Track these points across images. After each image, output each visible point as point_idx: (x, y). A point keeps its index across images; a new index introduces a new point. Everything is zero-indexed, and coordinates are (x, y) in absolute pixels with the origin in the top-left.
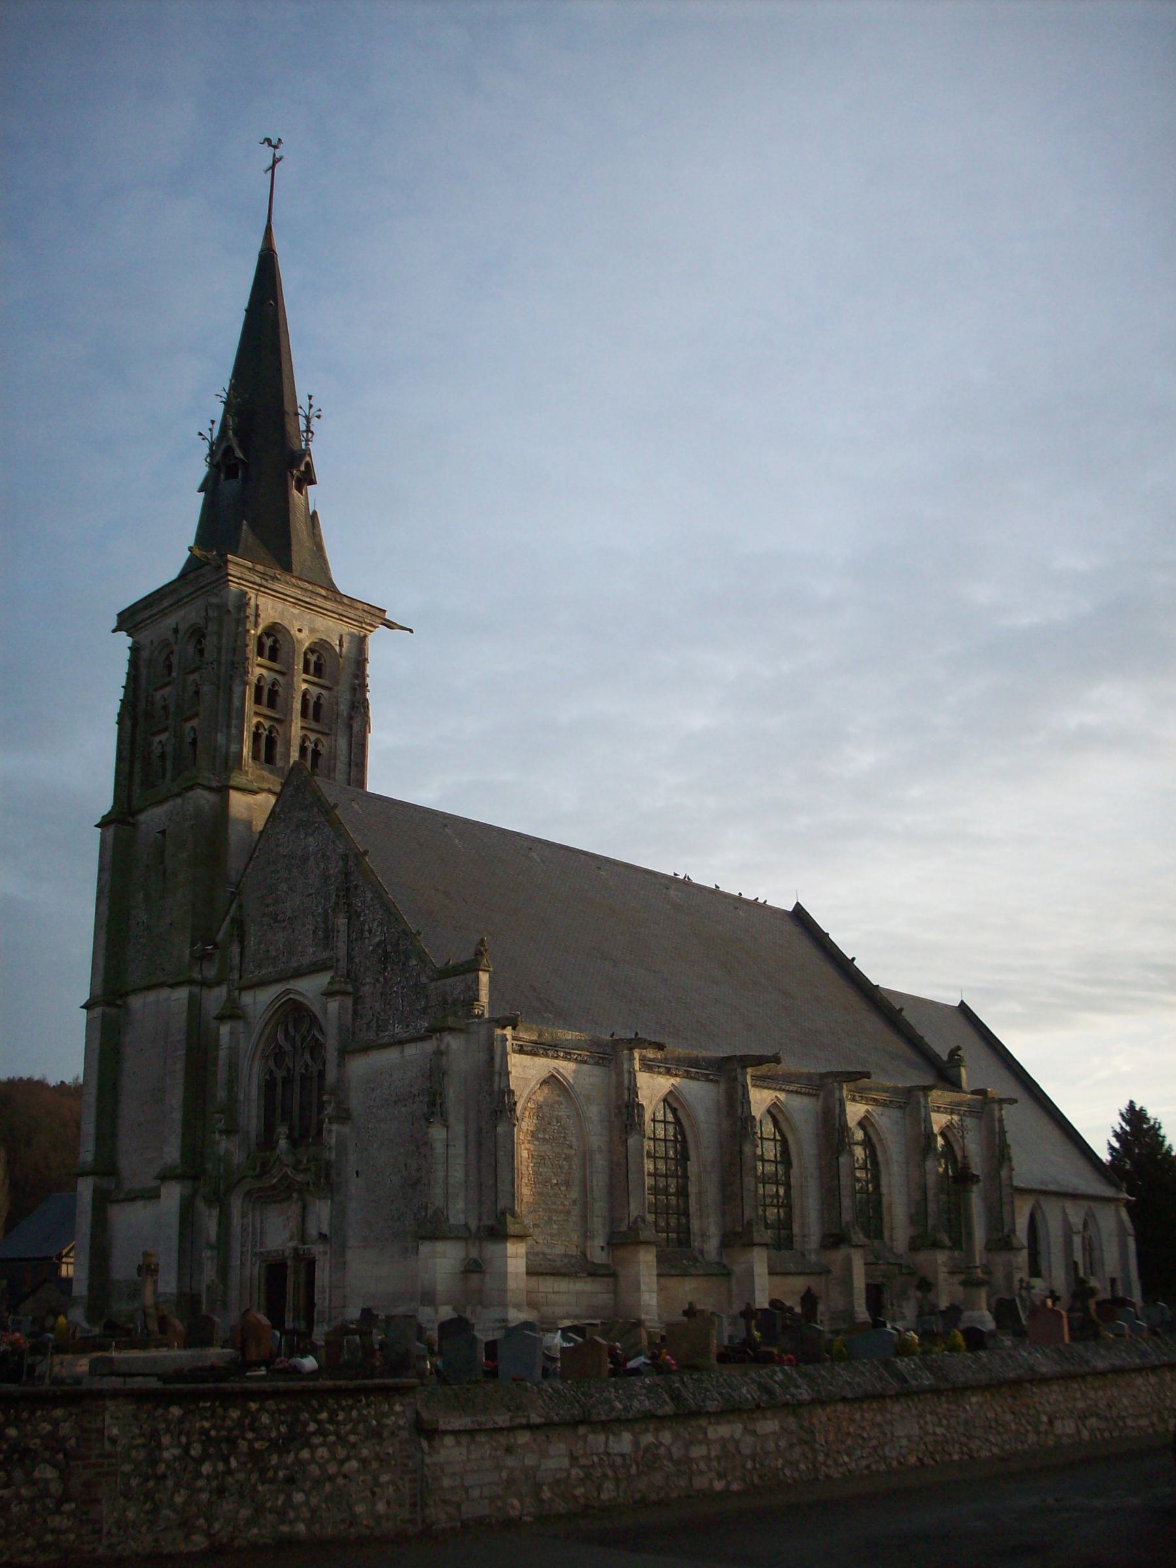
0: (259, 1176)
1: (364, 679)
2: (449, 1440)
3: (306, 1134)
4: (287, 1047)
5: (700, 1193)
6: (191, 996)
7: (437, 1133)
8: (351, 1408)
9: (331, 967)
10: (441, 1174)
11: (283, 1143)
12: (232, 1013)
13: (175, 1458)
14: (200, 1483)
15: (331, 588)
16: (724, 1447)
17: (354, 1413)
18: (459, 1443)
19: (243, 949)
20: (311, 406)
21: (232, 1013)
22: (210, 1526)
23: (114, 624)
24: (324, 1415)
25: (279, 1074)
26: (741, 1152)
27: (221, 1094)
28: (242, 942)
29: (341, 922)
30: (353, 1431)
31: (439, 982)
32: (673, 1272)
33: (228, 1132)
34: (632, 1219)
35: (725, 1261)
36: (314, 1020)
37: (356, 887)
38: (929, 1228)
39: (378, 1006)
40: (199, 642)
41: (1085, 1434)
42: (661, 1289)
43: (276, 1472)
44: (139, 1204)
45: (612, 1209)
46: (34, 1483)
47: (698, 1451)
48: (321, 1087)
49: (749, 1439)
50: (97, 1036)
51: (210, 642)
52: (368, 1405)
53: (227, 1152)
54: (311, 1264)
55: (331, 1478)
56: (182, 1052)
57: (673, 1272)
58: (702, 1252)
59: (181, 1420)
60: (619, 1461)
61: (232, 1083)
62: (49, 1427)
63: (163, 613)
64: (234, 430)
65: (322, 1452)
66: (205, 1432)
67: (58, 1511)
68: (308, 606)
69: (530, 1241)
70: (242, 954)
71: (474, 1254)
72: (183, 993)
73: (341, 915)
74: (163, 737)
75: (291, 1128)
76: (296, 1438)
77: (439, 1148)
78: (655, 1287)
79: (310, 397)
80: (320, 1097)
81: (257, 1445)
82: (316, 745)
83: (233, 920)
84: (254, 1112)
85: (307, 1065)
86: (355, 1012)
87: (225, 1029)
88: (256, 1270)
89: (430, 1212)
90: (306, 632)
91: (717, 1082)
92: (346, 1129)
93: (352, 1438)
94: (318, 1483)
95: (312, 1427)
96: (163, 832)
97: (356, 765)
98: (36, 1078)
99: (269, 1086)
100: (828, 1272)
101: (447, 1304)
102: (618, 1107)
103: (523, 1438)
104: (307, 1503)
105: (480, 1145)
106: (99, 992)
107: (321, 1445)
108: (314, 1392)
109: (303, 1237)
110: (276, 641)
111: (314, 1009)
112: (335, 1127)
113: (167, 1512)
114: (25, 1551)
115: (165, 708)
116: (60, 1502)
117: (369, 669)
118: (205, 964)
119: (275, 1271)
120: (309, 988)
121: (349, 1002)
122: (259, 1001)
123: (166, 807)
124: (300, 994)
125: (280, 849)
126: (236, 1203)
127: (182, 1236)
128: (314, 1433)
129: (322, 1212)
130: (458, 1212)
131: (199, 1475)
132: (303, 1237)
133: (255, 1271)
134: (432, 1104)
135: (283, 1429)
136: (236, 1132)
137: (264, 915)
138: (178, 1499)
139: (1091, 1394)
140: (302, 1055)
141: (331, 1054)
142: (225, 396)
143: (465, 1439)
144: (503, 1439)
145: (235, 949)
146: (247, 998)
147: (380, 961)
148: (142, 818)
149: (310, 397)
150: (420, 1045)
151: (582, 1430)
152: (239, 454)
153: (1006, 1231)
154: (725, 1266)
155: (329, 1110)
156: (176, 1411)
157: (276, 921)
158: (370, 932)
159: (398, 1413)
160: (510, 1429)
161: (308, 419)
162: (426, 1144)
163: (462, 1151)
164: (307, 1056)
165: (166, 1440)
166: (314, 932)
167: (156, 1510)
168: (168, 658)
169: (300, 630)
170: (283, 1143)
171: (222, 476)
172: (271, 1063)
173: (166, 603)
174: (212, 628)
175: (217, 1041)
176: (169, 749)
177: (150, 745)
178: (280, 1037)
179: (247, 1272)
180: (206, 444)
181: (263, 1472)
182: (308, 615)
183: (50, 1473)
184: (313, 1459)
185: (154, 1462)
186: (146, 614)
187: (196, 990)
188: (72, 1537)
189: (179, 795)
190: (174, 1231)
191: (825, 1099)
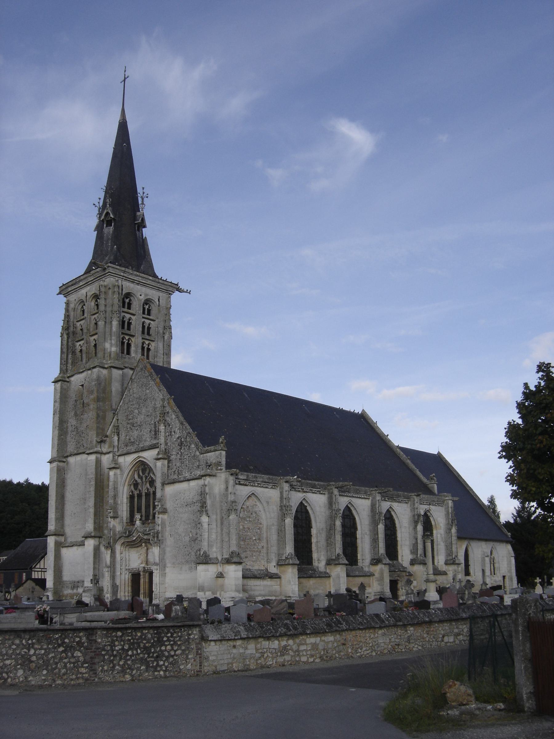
0: (128, 536)
1: (169, 316)
2: (213, 643)
3: (149, 518)
4: (139, 481)
5: (317, 542)
6: (97, 458)
7: (205, 519)
8: (179, 632)
9: (158, 447)
10: (206, 536)
11: (138, 523)
12: (116, 467)
13: (120, 649)
14: (128, 657)
15: (155, 276)
16: (313, 646)
17: (180, 634)
18: (216, 645)
19: (119, 438)
20: (144, 193)
21: (116, 467)
22: (132, 672)
23: (58, 291)
24: (169, 635)
25: (136, 493)
26: (334, 525)
27: (111, 501)
28: (118, 435)
29: (162, 427)
30: (180, 640)
31: (205, 455)
32: (305, 576)
33: (114, 517)
34: (287, 554)
35: (328, 571)
36: (151, 469)
37: (168, 413)
38: (419, 555)
40: (97, 301)
41: (457, 642)
42: (300, 583)
43: (153, 654)
44: (75, 548)
45: (279, 550)
46: (75, 657)
47: (302, 648)
48: (154, 499)
49: (322, 643)
50: (55, 475)
51: (101, 302)
52: (184, 631)
53: (114, 526)
54: (151, 574)
55: (172, 656)
56: (93, 483)
57: (305, 576)
58: (318, 567)
59: (121, 636)
60: (274, 651)
61: (115, 497)
62: (78, 639)
63: (81, 288)
64: (109, 204)
65: (169, 647)
66: (129, 640)
67: (82, 667)
68: (144, 285)
69: (243, 564)
70: (118, 440)
71: (220, 569)
72: (93, 457)
73: (162, 425)
74: (81, 343)
75: (141, 516)
76: (160, 642)
77: (205, 526)
79: (143, 188)
80: (154, 503)
81: (147, 645)
82: (149, 346)
83: (114, 426)
84: (125, 509)
85: (148, 489)
86: (168, 467)
87: (112, 473)
88: (127, 576)
89: (202, 553)
90: (143, 296)
91: (324, 494)
92: (165, 517)
93: (179, 643)
94: (167, 658)
95: (165, 639)
96: (82, 386)
97: (166, 355)
98: (8, 480)
99: (132, 497)
100: (374, 575)
101: (209, 591)
102: (281, 506)
103: (239, 643)
104: (164, 665)
105: (222, 524)
106: (55, 456)
107: (168, 645)
108: (144, 628)
109: (147, 563)
110: (130, 300)
111: (150, 465)
112: (161, 516)
113: (117, 667)
114: (72, 680)
115: (82, 330)
116: (82, 664)
117: (172, 311)
118: (103, 444)
119: (135, 577)
120: (149, 456)
121: (166, 462)
122: (127, 461)
123: (84, 374)
124: (144, 458)
125: (135, 395)
126: (118, 547)
127: (94, 563)
128: (166, 641)
129: (155, 551)
130: (215, 553)
131: (128, 655)
132: (147, 563)
133: (127, 577)
134: (202, 507)
135: (156, 639)
136: (117, 517)
137: (128, 423)
138: (121, 663)
139: (460, 627)
140: (146, 484)
141: (158, 484)
142: (105, 188)
143: (218, 643)
144: (231, 643)
145: (116, 438)
146: (121, 460)
147: (179, 445)
148: (72, 379)
149: (143, 188)
150: (196, 481)
151: (260, 640)
152: (112, 216)
153: (454, 556)
154: (328, 573)
155: (158, 509)
156: (119, 634)
157: (133, 426)
158: (175, 432)
159: (195, 633)
160: (234, 639)
161: (143, 199)
162: (199, 523)
163: (215, 527)
164: (148, 485)
165: (117, 643)
166: (150, 432)
167: (114, 666)
168: (82, 307)
169: (141, 295)
170: (138, 523)
171: (105, 225)
172: (132, 487)
173: (81, 284)
174: (102, 296)
175: (109, 478)
176: (84, 348)
177: (75, 346)
178: (136, 477)
179: (123, 579)
180: (97, 209)
181: (149, 654)
183: (79, 654)
184: (166, 650)
185: (113, 651)
186: (73, 287)
187: (99, 455)
188: (87, 675)
189: (89, 369)
190: (91, 559)
191: (372, 500)
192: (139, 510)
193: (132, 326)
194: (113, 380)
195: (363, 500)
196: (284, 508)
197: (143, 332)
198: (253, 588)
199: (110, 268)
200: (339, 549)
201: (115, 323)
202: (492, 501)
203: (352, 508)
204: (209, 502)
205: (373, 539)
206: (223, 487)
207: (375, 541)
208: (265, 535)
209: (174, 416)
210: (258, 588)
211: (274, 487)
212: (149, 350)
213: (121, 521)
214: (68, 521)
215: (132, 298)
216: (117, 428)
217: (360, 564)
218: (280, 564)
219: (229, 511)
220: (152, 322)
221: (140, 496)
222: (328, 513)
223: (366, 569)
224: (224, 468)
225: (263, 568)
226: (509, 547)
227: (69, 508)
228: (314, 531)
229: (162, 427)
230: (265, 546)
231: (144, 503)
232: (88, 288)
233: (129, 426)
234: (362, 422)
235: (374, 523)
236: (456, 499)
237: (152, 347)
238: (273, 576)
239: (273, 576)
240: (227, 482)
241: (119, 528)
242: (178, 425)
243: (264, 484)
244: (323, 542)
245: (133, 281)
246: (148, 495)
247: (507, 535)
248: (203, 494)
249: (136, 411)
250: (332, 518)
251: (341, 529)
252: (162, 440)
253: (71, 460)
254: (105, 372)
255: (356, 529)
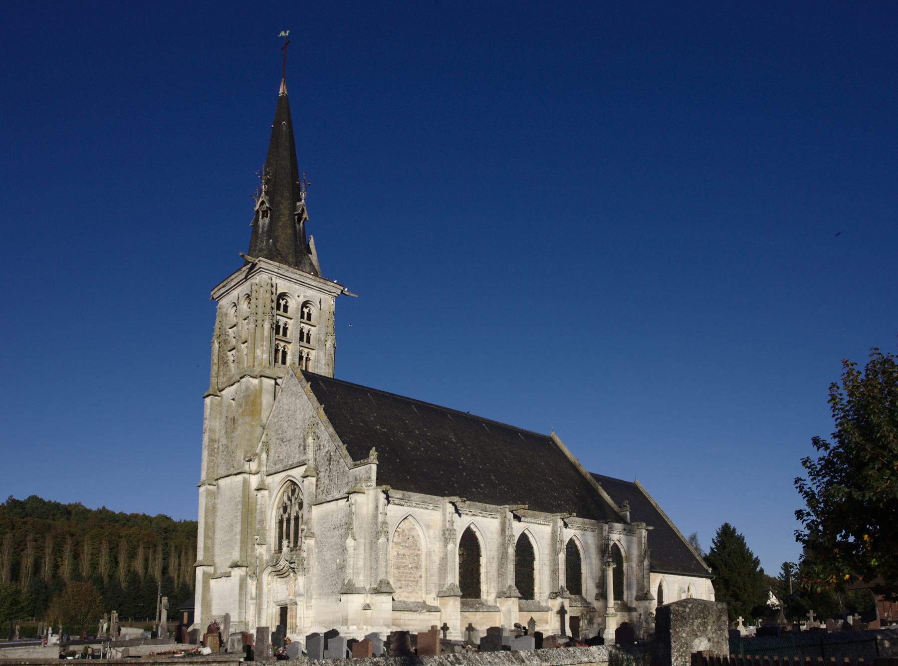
4: (288, 503)
7: (350, 542)
25: (286, 516)
29: (310, 440)
35: (498, 605)
39: (327, 482)
45: (440, 580)
58: (486, 601)
68: (302, 284)
71: (368, 602)
77: (351, 551)
78: (459, 617)
86: (317, 485)
99: (281, 522)
102: (444, 531)
110: (286, 302)
126: (266, 578)
130: (361, 581)
145: (264, 456)
152: (267, 205)
172: (282, 510)
178: (285, 499)
182: (302, 288)
190: (237, 591)
192: (288, 537)
193: (288, 332)
194: (264, 391)
195: (543, 527)
196: (447, 533)
197: (301, 339)
198: (407, 622)
199: (262, 263)
200: (511, 580)
201: (267, 326)
202: (693, 538)
203: (529, 536)
204: (355, 524)
205: (553, 571)
206: (371, 506)
207: (555, 572)
208: (423, 563)
209: (323, 428)
210: (412, 622)
211: (436, 507)
212: (308, 359)
213: (269, 549)
214: (217, 551)
215: (288, 299)
216: (266, 444)
217: (537, 597)
218: (441, 595)
219: (377, 535)
220: (312, 328)
221: (288, 520)
222: (500, 540)
223: (543, 604)
224: (374, 483)
225: (421, 600)
226: (708, 582)
227: (219, 536)
228: (483, 560)
229: (310, 440)
230: (423, 575)
231: (291, 529)
232: (240, 288)
233: (278, 441)
234: (546, 444)
235: (555, 552)
236: (651, 528)
237: (312, 357)
238: (431, 609)
239: (431, 609)
240: (377, 500)
241: (266, 557)
242: (327, 437)
243: (423, 504)
244: (494, 573)
245: (290, 279)
246: (297, 519)
247: (707, 571)
248: (350, 514)
249: (286, 425)
250: (504, 546)
251: (514, 558)
252: (310, 454)
253: (222, 482)
254: (255, 381)
255: (533, 559)
